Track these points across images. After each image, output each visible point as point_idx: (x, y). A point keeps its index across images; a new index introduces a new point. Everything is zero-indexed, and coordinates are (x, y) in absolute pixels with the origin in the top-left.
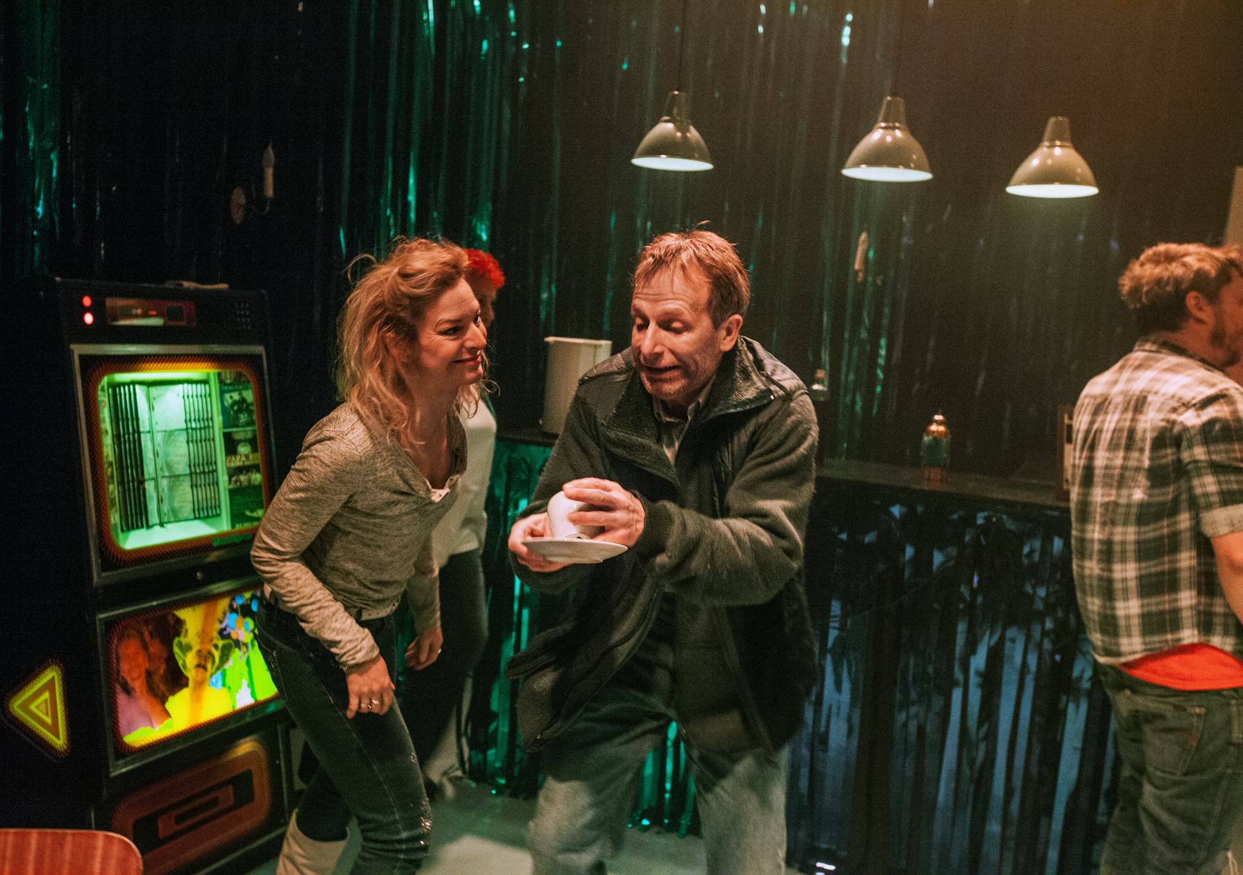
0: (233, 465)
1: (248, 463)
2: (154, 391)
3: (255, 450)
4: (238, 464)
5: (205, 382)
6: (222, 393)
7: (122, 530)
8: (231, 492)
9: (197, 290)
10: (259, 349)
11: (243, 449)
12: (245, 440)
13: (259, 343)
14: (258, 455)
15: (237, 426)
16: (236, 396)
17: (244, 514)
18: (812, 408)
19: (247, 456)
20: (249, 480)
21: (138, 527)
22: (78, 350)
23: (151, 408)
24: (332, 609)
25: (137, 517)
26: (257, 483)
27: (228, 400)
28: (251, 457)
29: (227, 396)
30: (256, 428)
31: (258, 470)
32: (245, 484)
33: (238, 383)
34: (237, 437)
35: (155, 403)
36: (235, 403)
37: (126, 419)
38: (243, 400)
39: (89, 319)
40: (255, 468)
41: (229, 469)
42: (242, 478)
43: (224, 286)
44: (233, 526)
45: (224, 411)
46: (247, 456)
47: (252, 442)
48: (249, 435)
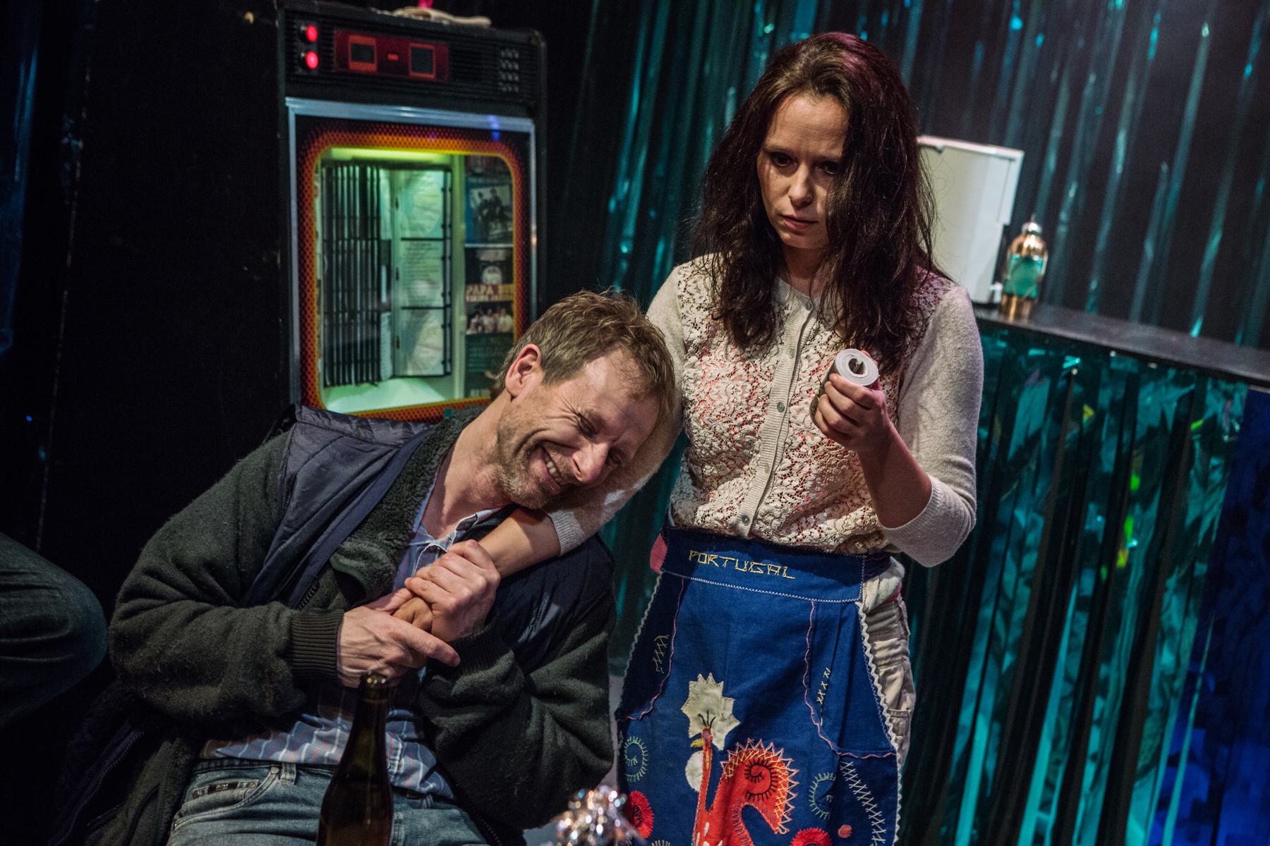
0: (474, 299)
1: (496, 298)
2: (402, 175)
3: (507, 279)
4: (483, 298)
5: (446, 168)
6: (468, 187)
7: (325, 386)
8: (469, 339)
9: (452, 25)
10: (525, 125)
11: (492, 277)
12: (494, 263)
13: (530, 113)
14: (513, 287)
15: (486, 241)
16: (487, 194)
17: (483, 374)
18: (981, 353)
19: (495, 288)
20: (495, 325)
21: (344, 383)
22: (296, 106)
23: (395, 204)
24: (272, 615)
25: (359, 364)
26: (505, 330)
27: (476, 197)
28: (501, 289)
29: (475, 192)
30: (513, 245)
31: (510, 313)
32: (489, 329)
33: (494, 171)
34: (484, 257)
35: (401, 199)
36: (485, 204)
37: (361, 215)
38: (496, 201)
39: (312, 60)
40: (506, 306)
41: (468, 304)
42: (486, 320)
43: (483, 21)
44: (467, 394)
45: (470, 216)
46: (495, 288)
47: (505, 266)
48: (501, 256)
